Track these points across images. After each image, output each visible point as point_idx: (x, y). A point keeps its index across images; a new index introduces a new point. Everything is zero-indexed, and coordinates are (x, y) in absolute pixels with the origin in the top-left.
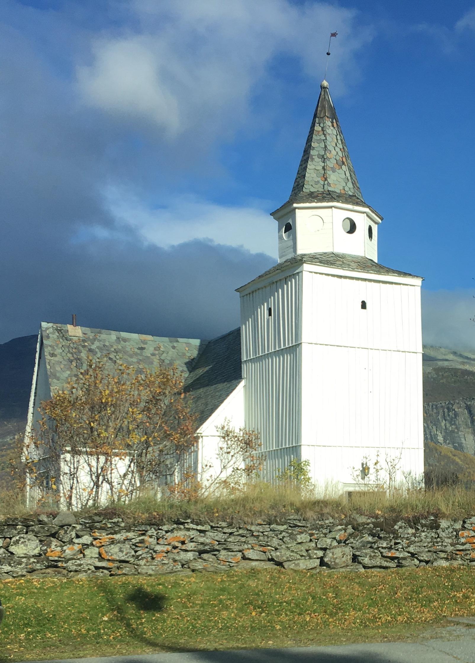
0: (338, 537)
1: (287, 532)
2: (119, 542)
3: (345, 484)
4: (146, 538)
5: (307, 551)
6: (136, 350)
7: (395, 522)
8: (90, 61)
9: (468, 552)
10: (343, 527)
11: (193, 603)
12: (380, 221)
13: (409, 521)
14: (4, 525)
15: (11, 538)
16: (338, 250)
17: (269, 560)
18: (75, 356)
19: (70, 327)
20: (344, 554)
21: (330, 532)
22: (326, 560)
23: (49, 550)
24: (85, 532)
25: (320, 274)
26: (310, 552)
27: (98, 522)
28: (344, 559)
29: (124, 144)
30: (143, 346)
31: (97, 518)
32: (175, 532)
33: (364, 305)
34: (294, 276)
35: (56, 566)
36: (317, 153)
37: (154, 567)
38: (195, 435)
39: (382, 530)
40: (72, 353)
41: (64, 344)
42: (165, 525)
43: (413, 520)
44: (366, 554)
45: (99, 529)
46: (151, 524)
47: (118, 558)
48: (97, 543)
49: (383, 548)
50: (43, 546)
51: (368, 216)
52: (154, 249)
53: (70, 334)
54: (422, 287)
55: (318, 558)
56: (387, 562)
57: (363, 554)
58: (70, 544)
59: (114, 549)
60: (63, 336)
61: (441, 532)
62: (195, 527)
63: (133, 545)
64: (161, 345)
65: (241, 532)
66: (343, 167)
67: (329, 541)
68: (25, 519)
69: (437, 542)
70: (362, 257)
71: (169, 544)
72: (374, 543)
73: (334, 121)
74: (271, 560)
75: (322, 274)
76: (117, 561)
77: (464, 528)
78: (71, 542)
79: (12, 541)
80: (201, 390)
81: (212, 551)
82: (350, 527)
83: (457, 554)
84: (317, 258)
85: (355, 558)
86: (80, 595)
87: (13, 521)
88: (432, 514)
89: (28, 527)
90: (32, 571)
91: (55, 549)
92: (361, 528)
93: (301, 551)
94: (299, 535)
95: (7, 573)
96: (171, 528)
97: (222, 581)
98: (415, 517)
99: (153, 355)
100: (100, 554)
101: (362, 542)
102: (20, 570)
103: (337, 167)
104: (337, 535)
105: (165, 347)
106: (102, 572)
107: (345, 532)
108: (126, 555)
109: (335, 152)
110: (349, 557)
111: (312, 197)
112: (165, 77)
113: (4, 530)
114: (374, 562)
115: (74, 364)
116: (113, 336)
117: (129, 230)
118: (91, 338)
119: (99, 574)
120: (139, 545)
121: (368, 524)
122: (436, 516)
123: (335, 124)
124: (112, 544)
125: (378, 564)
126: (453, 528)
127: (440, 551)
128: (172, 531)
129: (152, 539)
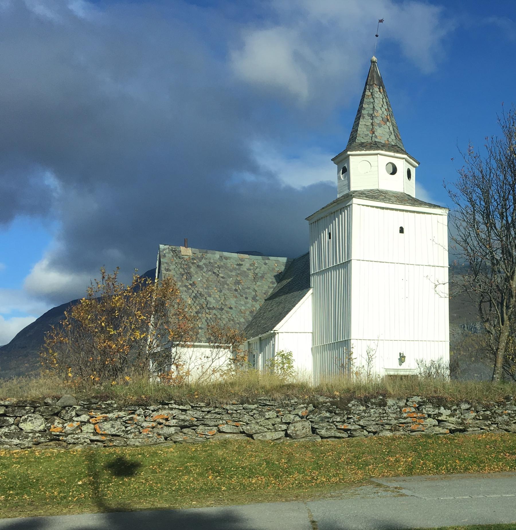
0: (300, 414)
1: (257, 410)
2: (111, 420)
3: (386, 370)
4: (134, 416)
5: (273, 425)
6: (235, 266)
7: (349, 401)
8: (241, 46)
9: (409, 425)
10: (305, 405)
11: (162, 469)
12: (417, 165)
13: (361, 400)
14: (16, 407)
15: (21, 417)
16: (383, 187)
17: (241, 433)
18: (185, 270)
19: (182, 249)
20: (304, 427)
21: (294, 409)
22: (289, 432)
23: (52, 426)
24: (84, 412)
25: (366, 206)
26: (276, 425)
27: (95, 404)
28: (304, 431)
29: (266, 110)
30: (241, 263)
31: (93, 401)
32: (160, 411)
33: (402, 230)
34: (346, 207)
35: (59, 440)
36: (367, 112)
37: (140, 440)
38: (272, 332)
39: (337, 408)
40: (183, 269)
41: (177, 261)
42: (151, 405)
43: (365, 400)
44: (323, 427)
45: (95, 409)
46: (139, 405)
47: (110, 433)
48: (93, 421)
49: (337, 422)
50: (48, 423)
51: (406, 160)
52: (289, 190)
53: (182, 253)
54: (449, 216)
55: (283, 431)
56: (340, 433)
57: (320, 427)
58: (70, 422)
59: (107, 426)
60: (177, 255)
61: (388, 409)
62: (177, 407)
63: (124, 422)
64: (256, 261)
65: (217, 410)
66: (388, 123)
67: (292, 417)
68: (33, 402)
69: (383, 417)
70: (401, 193)
71: (155, 421)
72: (330, 418)
73: (381, 87)
74: (243, 432)
75: (368, 206)
76: (109, 435)
77: (406, 405)
78: (71, 420)
79: (22, 419)
80: (283, 297)
81: (191, 426)
82: (311, 405)
83: (400, 427)
84: (365, 194)
85: (314, 430)
86: (67, 463)
87: (23, 403)
88: (381, 395)
89: (35, 408)
90: (37, 444)
91: (57, 426)
92: (320, 406)
93: (268, 425)
94: (268, 412)
95: (16, 445)
96: (156, 408)
97: (196, 450)
98: (366, 397)
99: (249, 269)
100: (95, 429)
101: (320, 417)
102: (26, 443)
103: (382, 123)
104: (299, 412)
105: (259, 263)
106: (96, 444)
107: (307, 409)
108: (117, 430)
109: (381, 111)
110: (308, 430)
111: (363, 146)
112: (297, 57)
113: (15, 410)
114: (329, 434)
115: (185, 277)
116: (217, 255)
117: (270, 175)
118: (199, 256)
119: (94, 446)
120: (129, 422)
121: (326, 403)
122: (384, 396)
123: (382, 90)
124: (106, 421)
125: (333, 435)
126: (398, 406)
127: (386, 424)
128: (157, 410)
129: (140, 417)
